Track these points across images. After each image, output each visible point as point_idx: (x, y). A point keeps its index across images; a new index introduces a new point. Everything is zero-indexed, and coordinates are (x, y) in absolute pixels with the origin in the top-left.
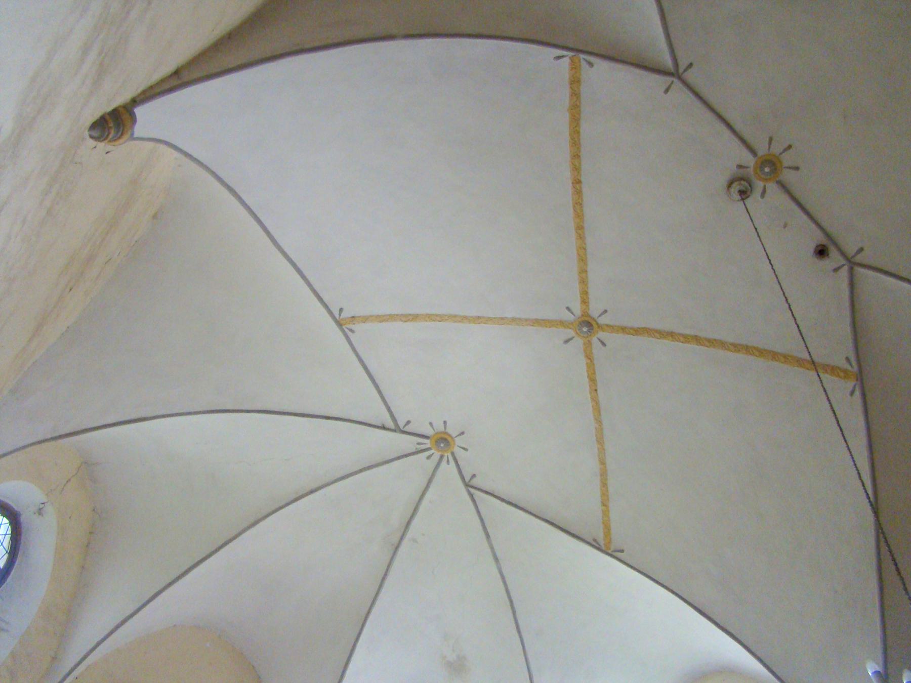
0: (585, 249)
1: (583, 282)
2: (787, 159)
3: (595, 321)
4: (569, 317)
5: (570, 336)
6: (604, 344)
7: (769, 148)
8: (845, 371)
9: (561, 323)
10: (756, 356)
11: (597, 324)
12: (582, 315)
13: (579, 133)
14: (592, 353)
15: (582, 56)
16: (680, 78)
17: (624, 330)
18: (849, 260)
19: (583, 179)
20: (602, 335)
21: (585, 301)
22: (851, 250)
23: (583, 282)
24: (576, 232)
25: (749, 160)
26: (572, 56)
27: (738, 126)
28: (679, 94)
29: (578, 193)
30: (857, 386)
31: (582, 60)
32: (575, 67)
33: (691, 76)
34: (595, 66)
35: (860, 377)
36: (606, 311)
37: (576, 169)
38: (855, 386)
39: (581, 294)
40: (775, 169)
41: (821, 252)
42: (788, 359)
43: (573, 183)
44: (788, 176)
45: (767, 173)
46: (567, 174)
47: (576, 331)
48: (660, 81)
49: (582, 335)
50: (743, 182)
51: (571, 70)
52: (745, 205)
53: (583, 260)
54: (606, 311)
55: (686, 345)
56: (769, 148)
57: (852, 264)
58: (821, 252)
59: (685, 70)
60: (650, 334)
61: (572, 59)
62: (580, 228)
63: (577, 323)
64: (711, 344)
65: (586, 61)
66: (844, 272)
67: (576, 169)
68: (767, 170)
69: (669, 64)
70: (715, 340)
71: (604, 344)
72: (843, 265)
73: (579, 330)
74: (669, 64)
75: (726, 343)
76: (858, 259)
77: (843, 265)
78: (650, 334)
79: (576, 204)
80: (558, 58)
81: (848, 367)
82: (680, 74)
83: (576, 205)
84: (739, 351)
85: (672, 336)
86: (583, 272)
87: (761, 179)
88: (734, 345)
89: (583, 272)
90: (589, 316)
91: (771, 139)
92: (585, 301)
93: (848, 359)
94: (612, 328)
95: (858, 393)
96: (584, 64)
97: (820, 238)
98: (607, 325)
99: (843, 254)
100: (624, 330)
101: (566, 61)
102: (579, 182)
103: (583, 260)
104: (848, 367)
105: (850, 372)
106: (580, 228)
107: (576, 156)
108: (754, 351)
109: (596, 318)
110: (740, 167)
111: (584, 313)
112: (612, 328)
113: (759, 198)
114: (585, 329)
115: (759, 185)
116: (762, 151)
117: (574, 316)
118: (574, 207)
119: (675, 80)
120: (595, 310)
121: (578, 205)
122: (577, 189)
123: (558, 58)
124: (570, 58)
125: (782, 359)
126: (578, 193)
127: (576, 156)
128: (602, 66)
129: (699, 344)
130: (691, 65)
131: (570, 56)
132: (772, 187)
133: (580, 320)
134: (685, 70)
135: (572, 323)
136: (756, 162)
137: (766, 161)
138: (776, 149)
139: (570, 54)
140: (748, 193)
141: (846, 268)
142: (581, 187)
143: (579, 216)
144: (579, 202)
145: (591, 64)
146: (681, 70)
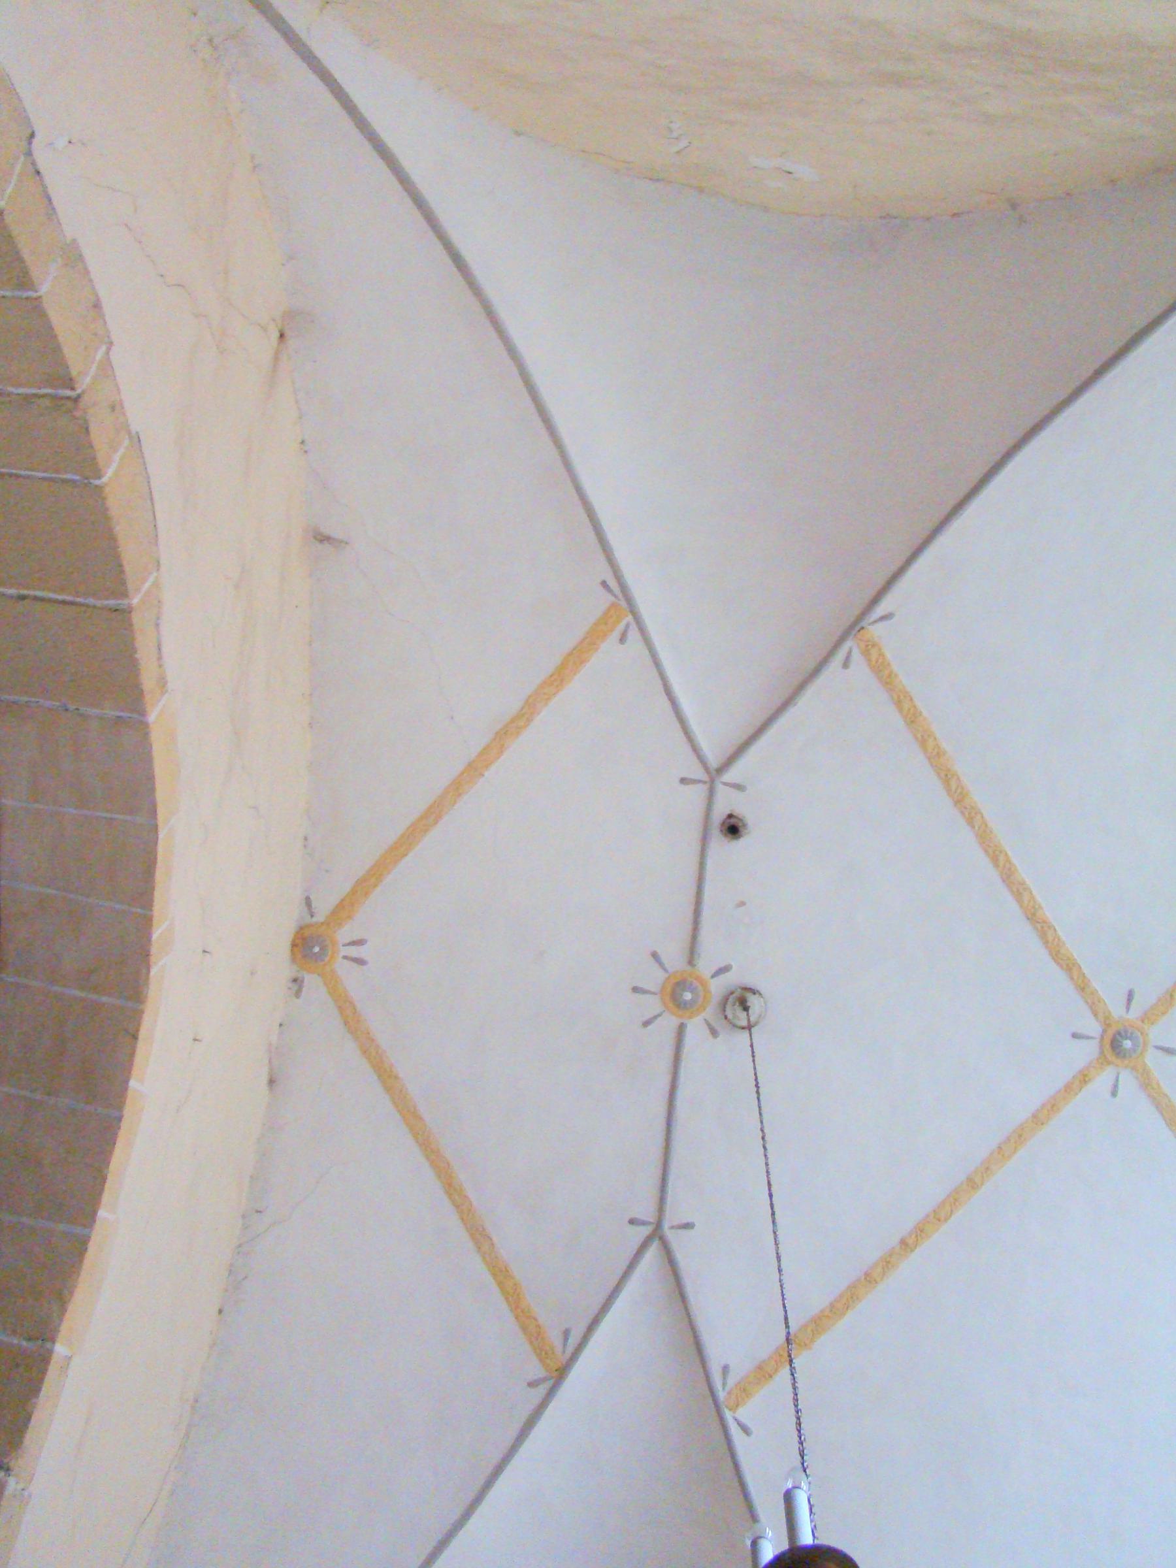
0: (1000, 1148)
1: (1052, 1106)
2: (654, 978)
3: (1102, 1037)
4: (1128, 1081)
5: (1159, 1053)
6: (1130, 996)
7: (656, 1017)
8: (866, 653)
9: (1147, 1083)
10: (958, 779)
11: (1104, 1031)
12: (1109, 1063)
13: (832, 1305)
14: (1159, 1000)
15: (721, 1395)
16: (659, 1225)
17: (1083, 987)
18: (712, 781)
19: (895, 1240)
20: (1116, 1009)
21: (1083, 1078)
22: (697, 794)
23: (1052, 1106)
24: (982, 1184)
25: (696, 1028)
26: (730, 1410)
27: (664, 1081)
28: (680, 1207)
29: (920, 1232)
30: (872, 620)
31: (728, 1388)
32: (744, 1392)
33: (645, 1209)
34: (723, 1363)
35: (855, 627)
36: (1075, 1036)
37: (887, 1263)
38: (870, 624)
39: (1077, 1094)
40: (677, 984)
41: (733, 829)
42: (922, 736)
43: (912, 1251)
44: (674, 955)
45: (691, 992)
46: (907, 1268)
47: (1141, 1053)
48: (684, 1247)
49: (1141, 1040)
50: (730, 1016)
51: (750, 1394)
52: (662, 1200)
53: (1018, 1137)
54: (1075, 1036)
55: (1029, 882)
56: (656, 1017)
57: (714, 774)
58: (733, 829)
59: (643, 1223)
60: (1058, 945)
61: (733, 1409)
62: (972, 1184)
63: (1126, 1062)
64: (997, 852)
65: (724, 1384)
66: (733, 775)
67: (887, 1263)
68: (688, 996)
69: (653, 1252)
70: (986, 851)
71: (1130, 996)
72: (725, 784)
73: (1135, 1051)
74: (653, 1252)
75: (977, 835)
76: (700, 774)
77: (725, 784)
78: (1058, 945)
79: (939, 1220)
80: (746, 1430)
81: (856, 655)
82: (655, 1226)
83: (943, 1219)
84: (972, 808)
85: (1034, 914)
86: (1038, 1119)
87: (707, 991)
88: (970, 821)
89: (1038, 1119)
90: (1102, 1052)
91: (646, 1024)
92: (1083, 1078)
93: (846, 664)
94: (1094, 1005)
95: (880, 610)
96: (731, 1382)
97: (720, 845)
98: (1095, 1014)
99: (711, 793)
100: (1083, 987)
101: (743, 1413)
102: (903, 1242)
103: (1018, 1137)
104: (856, 655)
105: (858, 646)
106: (972, 1184)
107: (869, 1279)
108: (954, 788)
109: (1098, 1040)
110: (714, 1033)
111: (1102, 1064)
112: (1094, 1005)
113: (734, 966)
114: (1127, 1044)
115: (718, 987)
116: (669, 1022)
117: (1118, 1074)
118: (946, 1220)
119: (666, 1225)
120: (1086, 1052)
121: (938, 1216)
122: (917, 1236)
123: (746, 1430)
124: (734, 1412)
125: (930, 743)
126: (920, 1232)
127: (869, 1279)
128: (716, 1355)
129: (1013, 869)
130: (632, 1222)
131: (731, 1413)
132: (705, 966)
133: (1118, 1061)
134: (643, 1223)
135: (1134, 1069)
136: (690, 1017)
137: (678, 1006)
138: (652, 1005)
139: (728, 1415)
140: (738, 993)
141: (728, 777)
142: (910, 1234)
143: (956, 1200)
144: (934, 1217)
145: (725, 1369)
146: (646, 1231)
